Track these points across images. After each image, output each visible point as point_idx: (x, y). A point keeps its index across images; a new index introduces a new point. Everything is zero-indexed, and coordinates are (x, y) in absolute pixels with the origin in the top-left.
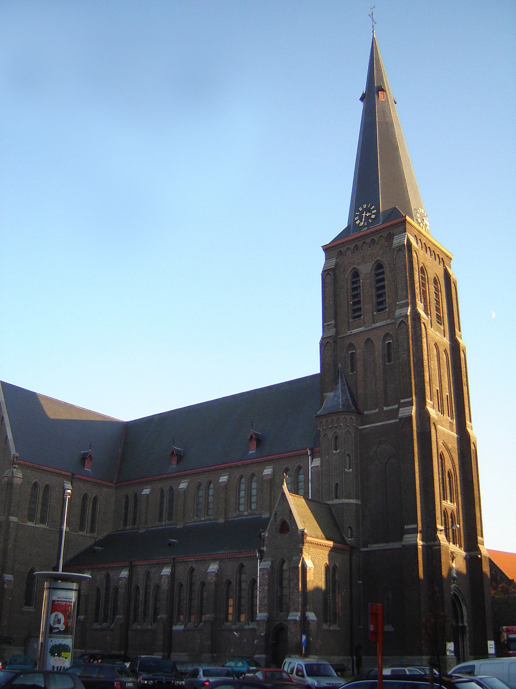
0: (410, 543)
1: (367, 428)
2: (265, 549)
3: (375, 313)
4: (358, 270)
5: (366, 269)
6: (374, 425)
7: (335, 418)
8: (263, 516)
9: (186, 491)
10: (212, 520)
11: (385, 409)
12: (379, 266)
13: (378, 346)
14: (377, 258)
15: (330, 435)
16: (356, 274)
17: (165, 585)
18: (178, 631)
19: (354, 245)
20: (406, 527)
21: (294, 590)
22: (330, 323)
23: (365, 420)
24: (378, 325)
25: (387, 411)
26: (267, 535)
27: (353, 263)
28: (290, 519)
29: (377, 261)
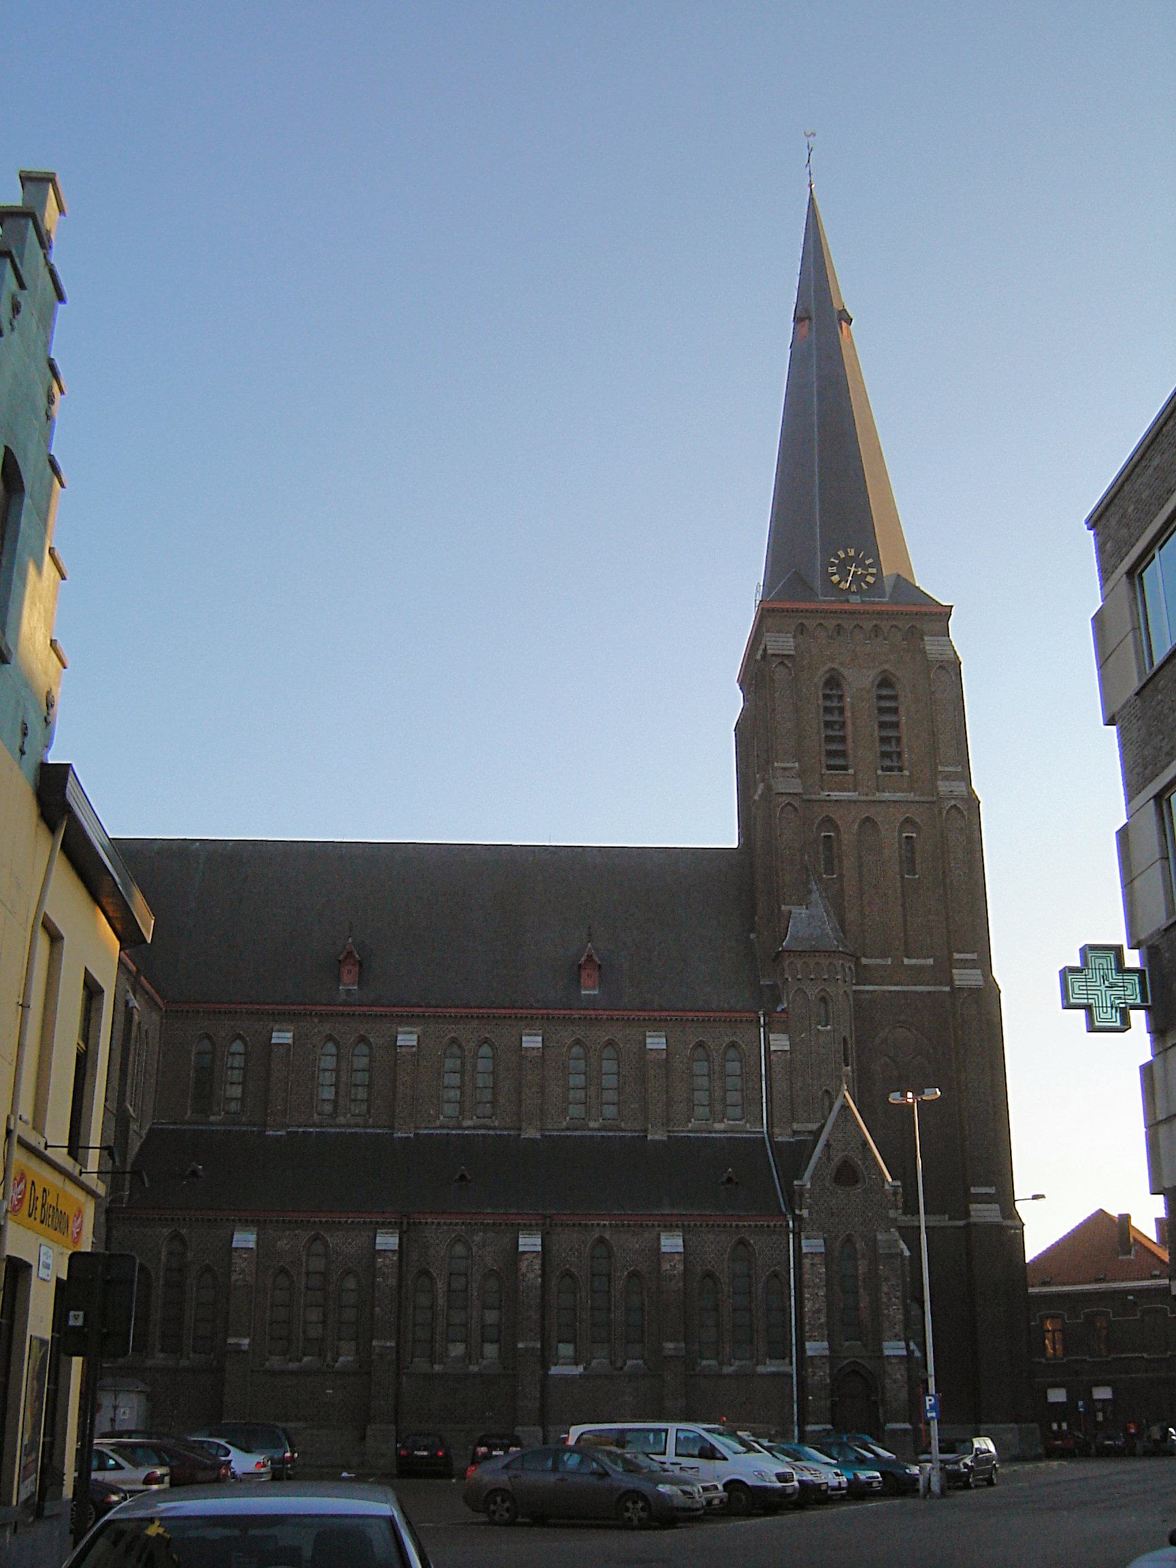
0: (989, 1219)
1: (868, 992)
2: (805, 1213)
3: (879, 772)
4: (839, 673)
5: (859, 682)
6: (885, 988)
7: (824, 962)
8: (650, 1137)
9: (417, 1054)
10: (494, 1128)
11: (906, 961)
12: (885, 682)
13: (890, 837)
14: (886, 667)
15: (813, 992)
16: (833, 681)
17: (531, 1272)
18: (566, 1379)
19: (835, 622)
20: (973, 1190)
21: (890, 1299)
22: (788, 765)
23: (862, 974)
24: (886, 796)
25: (910, 967)
26: (809, 1186)
27: (832, 660)
28: (864, 1159)
29: (885, 671)
